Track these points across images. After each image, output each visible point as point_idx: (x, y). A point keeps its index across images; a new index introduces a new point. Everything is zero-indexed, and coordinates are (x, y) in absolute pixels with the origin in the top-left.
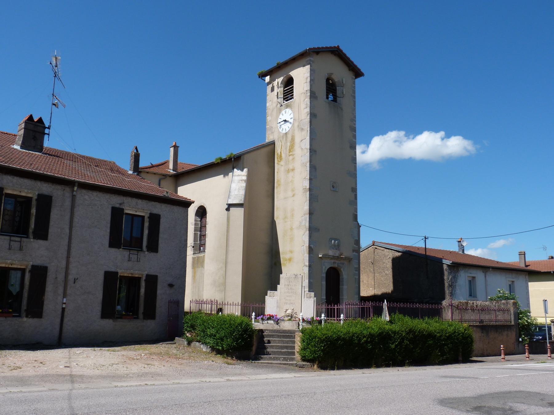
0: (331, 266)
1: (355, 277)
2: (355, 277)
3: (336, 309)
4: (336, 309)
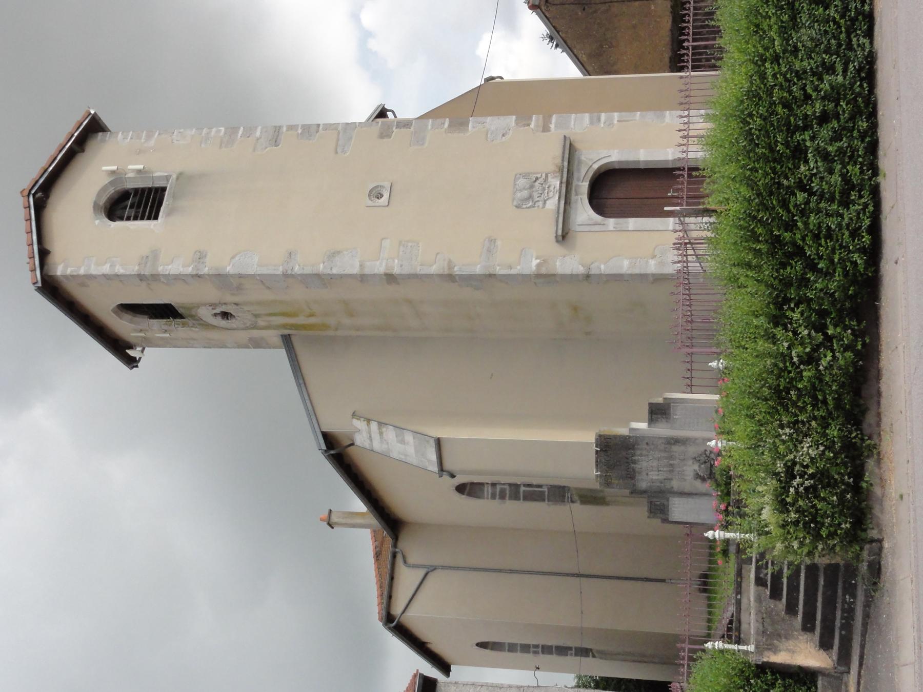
0: (586, 201)
1: (615, 122)
2: (615, 122)
3: (695, 44)
4: (695, 44)
